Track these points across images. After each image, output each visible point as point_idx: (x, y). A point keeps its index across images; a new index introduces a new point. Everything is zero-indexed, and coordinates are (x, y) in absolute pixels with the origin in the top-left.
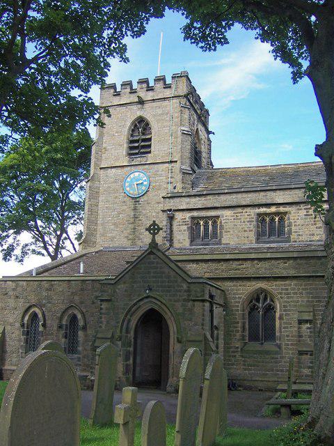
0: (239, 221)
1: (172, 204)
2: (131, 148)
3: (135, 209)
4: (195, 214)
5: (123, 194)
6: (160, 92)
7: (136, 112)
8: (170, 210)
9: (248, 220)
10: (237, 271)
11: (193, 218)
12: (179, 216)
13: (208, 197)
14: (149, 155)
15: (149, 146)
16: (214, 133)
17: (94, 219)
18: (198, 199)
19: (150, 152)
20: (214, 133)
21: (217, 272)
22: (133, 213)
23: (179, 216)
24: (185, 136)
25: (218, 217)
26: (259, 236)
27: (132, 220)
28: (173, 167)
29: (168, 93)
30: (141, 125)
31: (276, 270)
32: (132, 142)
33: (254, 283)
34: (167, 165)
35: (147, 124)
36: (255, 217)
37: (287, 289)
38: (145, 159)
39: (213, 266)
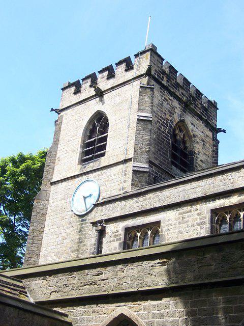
0: (186, 225)
1: (101, 214)
2: (87, 153)
3: (81, 231)
4: (130, 223)
5: (71, 213)
6: (121, 74)
7: (94, 106)
8: (100, 222)
9: (198, 221)
10: (93, 286)
11: (127, 230)
12: (110, 228)
13: (148, 196)
14: (103, 158)
15: (104, 147)
16: (224, 131)
17: (36, 249)
18: (135, 200)
19: (103, 155)
20: (224, 131)
21: (67, 289)
22: (78, 237)
23: (110, 228)
24: (142, 123)
25: (158, 223)
26: (158, 223)
27: (76, 246)
28: (127, 167)
29: (131, 75)
30: (99, 123)
31: (148, 279)
32: (88, 145)
33: (113, 306)
34: (121, 166)
35: (106, 120)
36: (208, 216)
37: (162, 316)
38: (97, 163)
39: (63, 278)
